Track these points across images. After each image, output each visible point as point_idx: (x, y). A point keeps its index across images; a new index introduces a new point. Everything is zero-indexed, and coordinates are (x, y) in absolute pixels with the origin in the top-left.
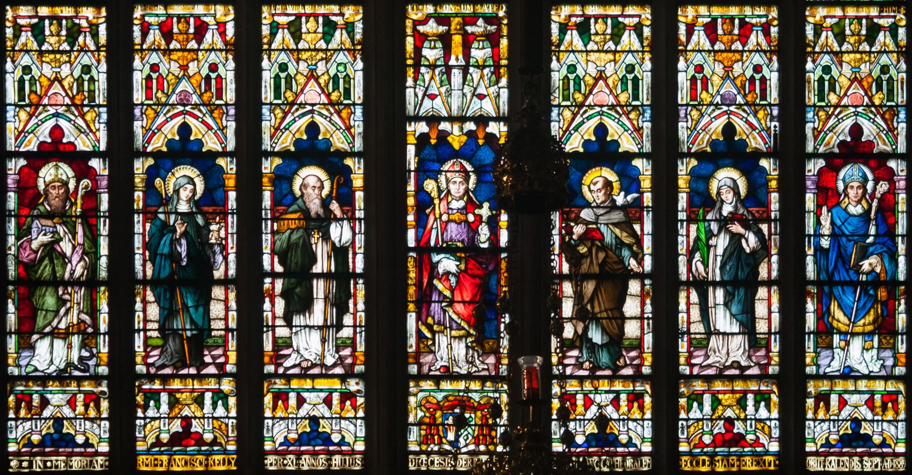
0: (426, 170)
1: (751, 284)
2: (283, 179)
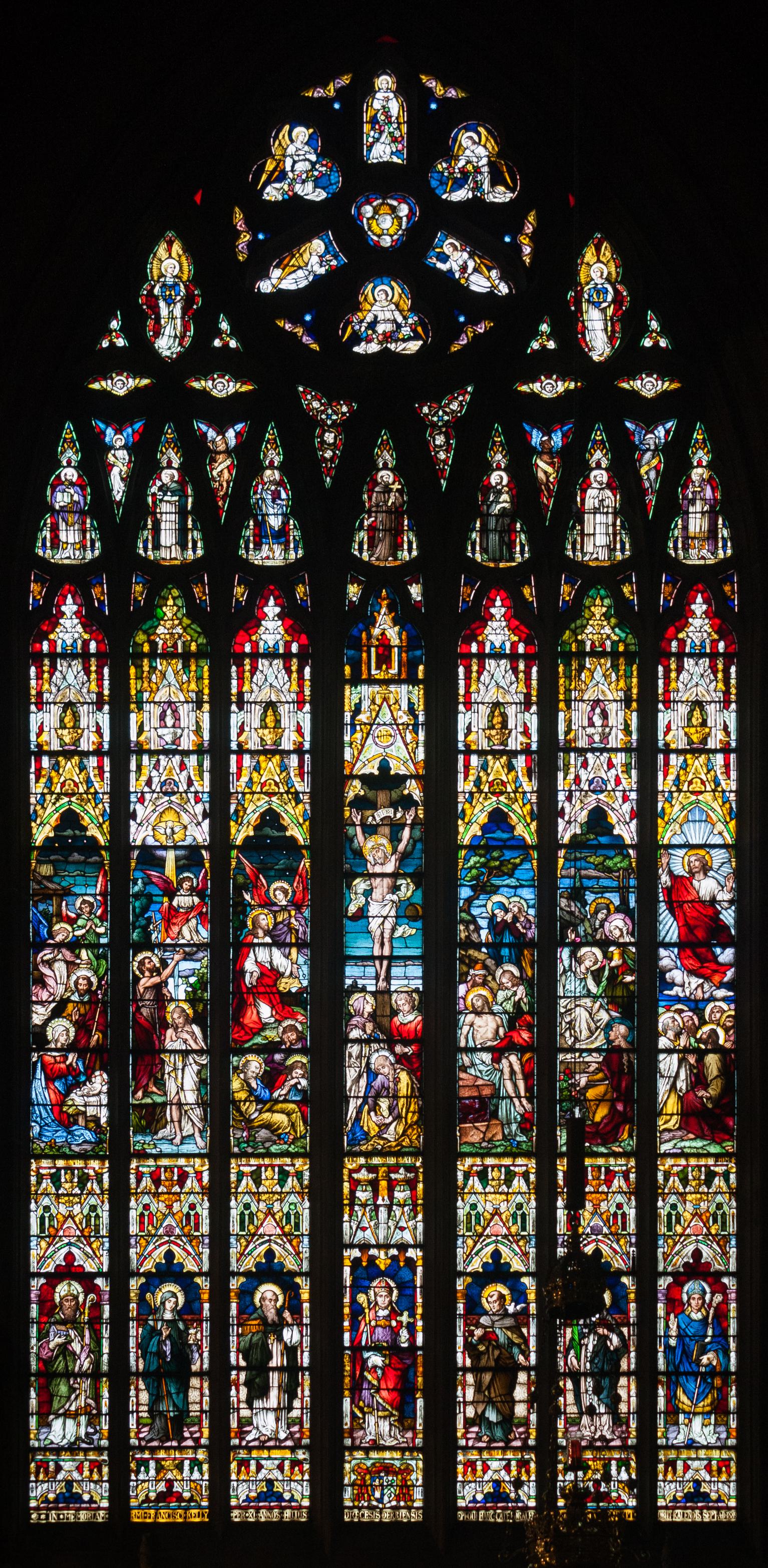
0: (359, 1286)
1: (616, 1374)
2: (246, 1293)
